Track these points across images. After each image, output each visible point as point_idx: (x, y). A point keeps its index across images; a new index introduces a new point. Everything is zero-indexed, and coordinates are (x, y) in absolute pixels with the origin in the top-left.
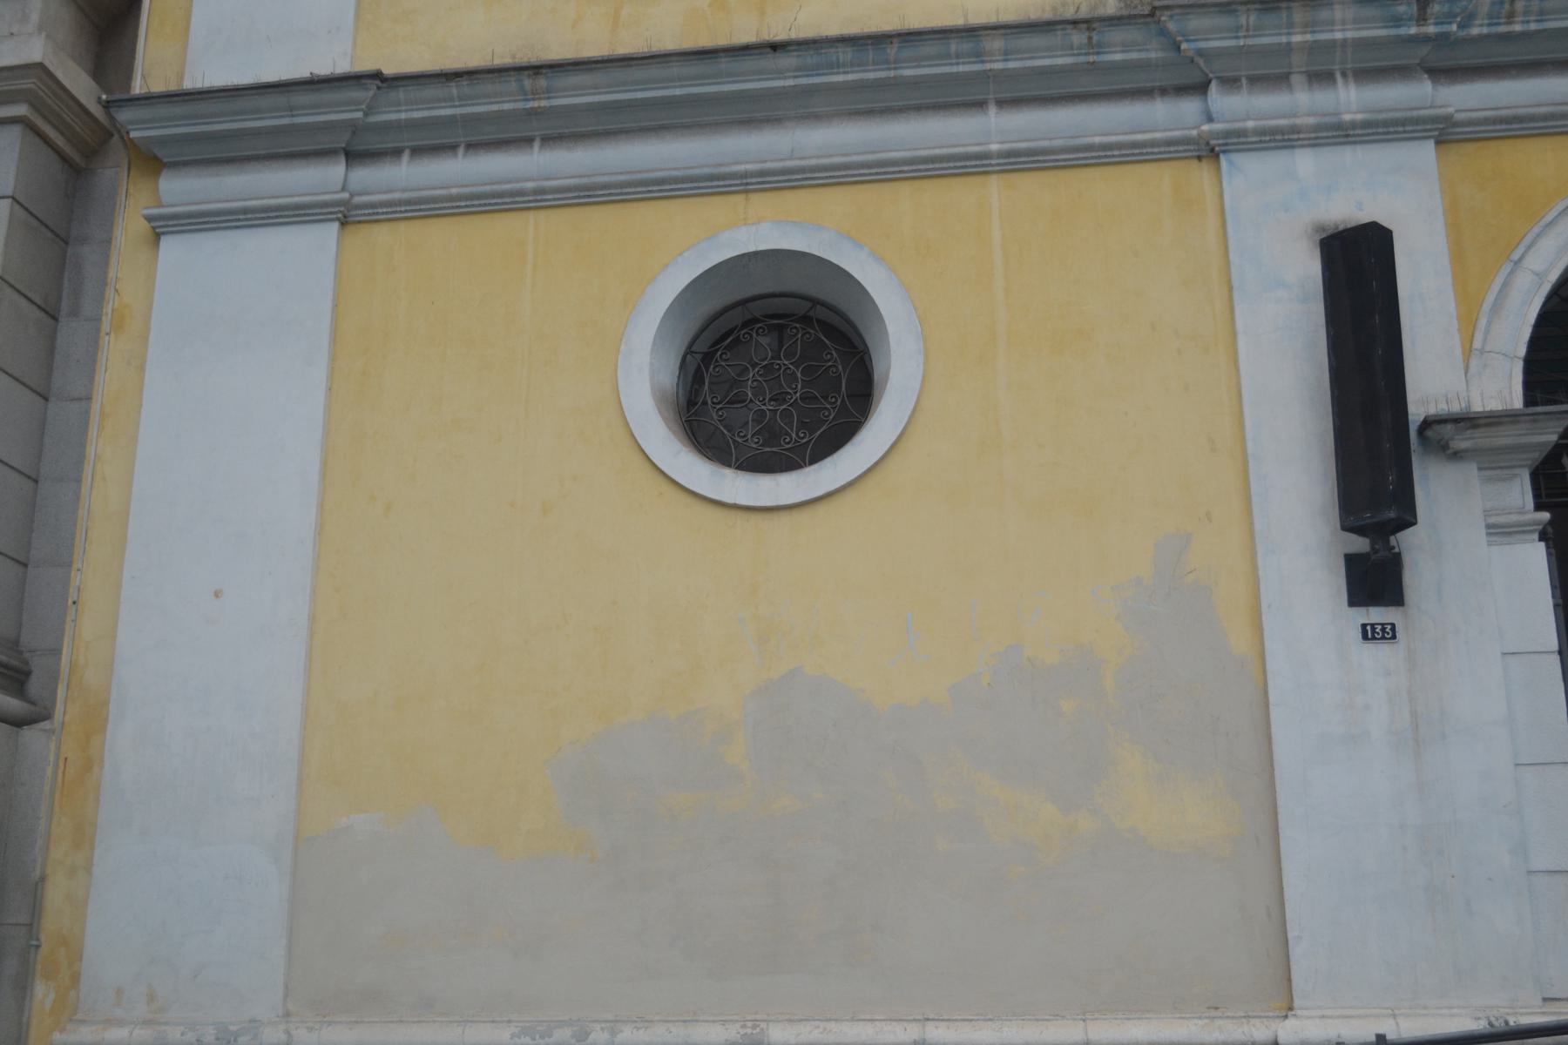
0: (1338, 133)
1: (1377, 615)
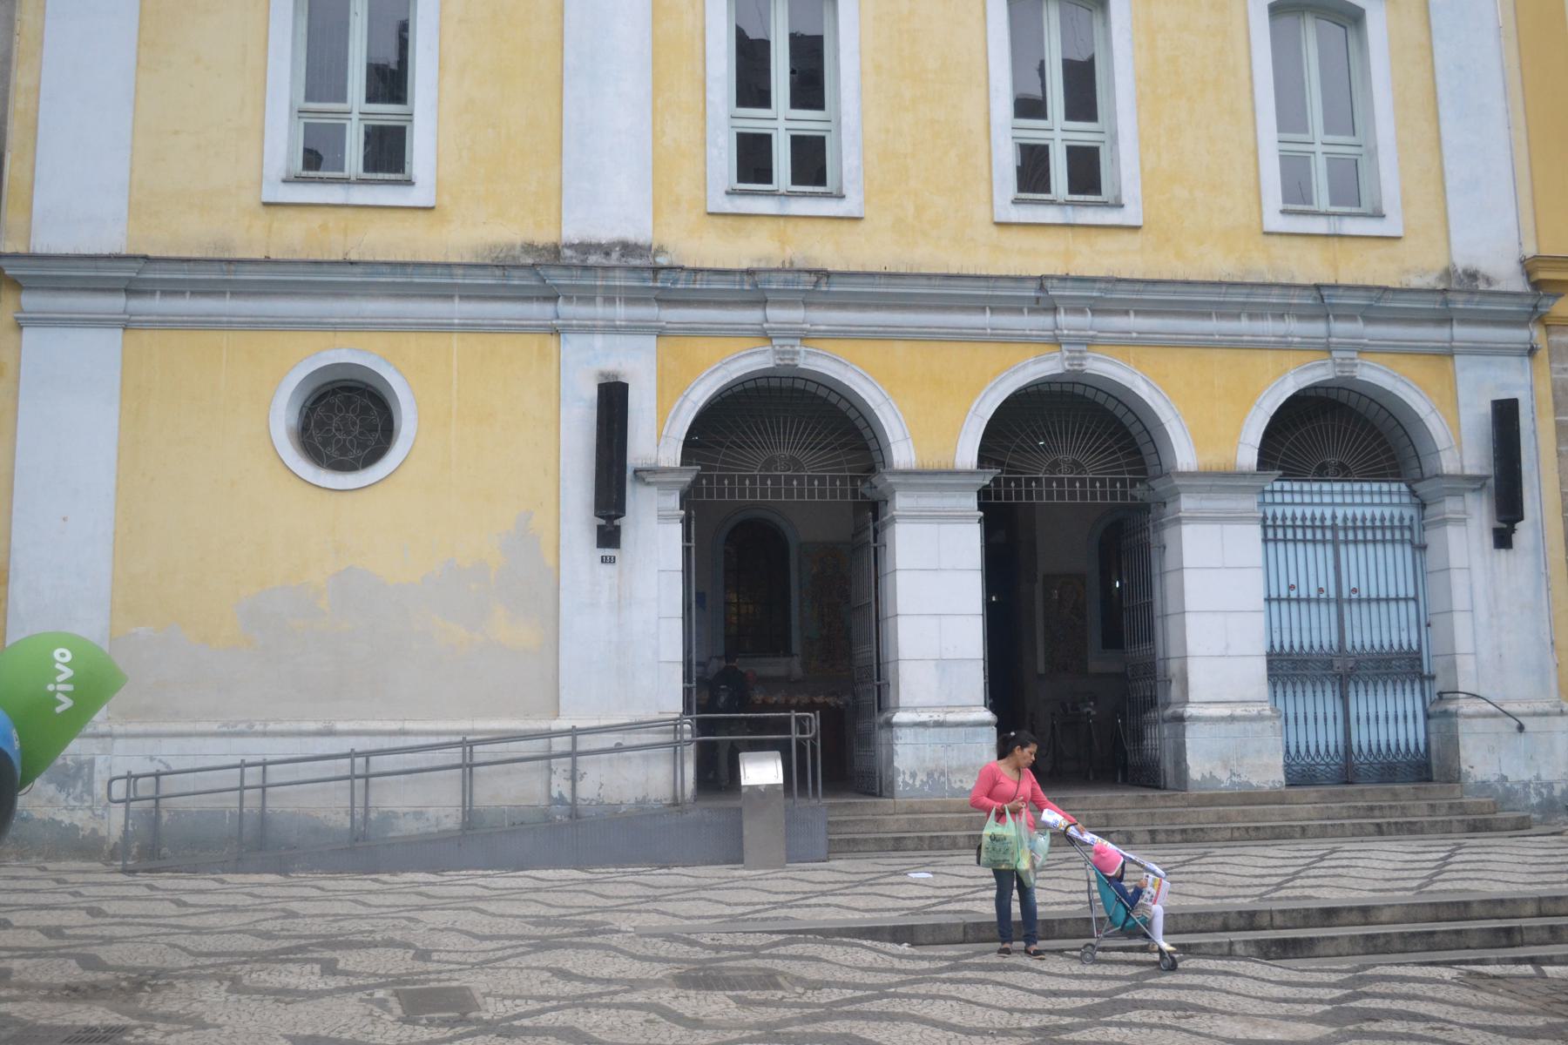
0: (613, 329)
1: (608, 552)
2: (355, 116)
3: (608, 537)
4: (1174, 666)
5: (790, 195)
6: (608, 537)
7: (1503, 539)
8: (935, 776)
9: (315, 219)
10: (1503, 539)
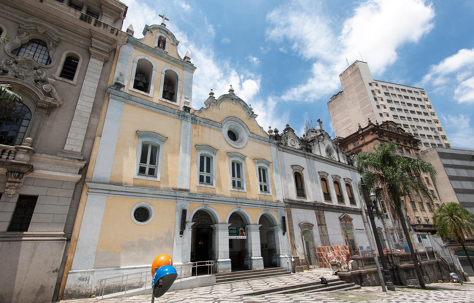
1: (181, 235)
2: (148, 166)
3: (181, 233)
4: (216, 253)
5: (147, 176)
6: (181, 233)
7: (284, 234)
8: (225, 269)
9: (142, 181)
10: (284, 234)
